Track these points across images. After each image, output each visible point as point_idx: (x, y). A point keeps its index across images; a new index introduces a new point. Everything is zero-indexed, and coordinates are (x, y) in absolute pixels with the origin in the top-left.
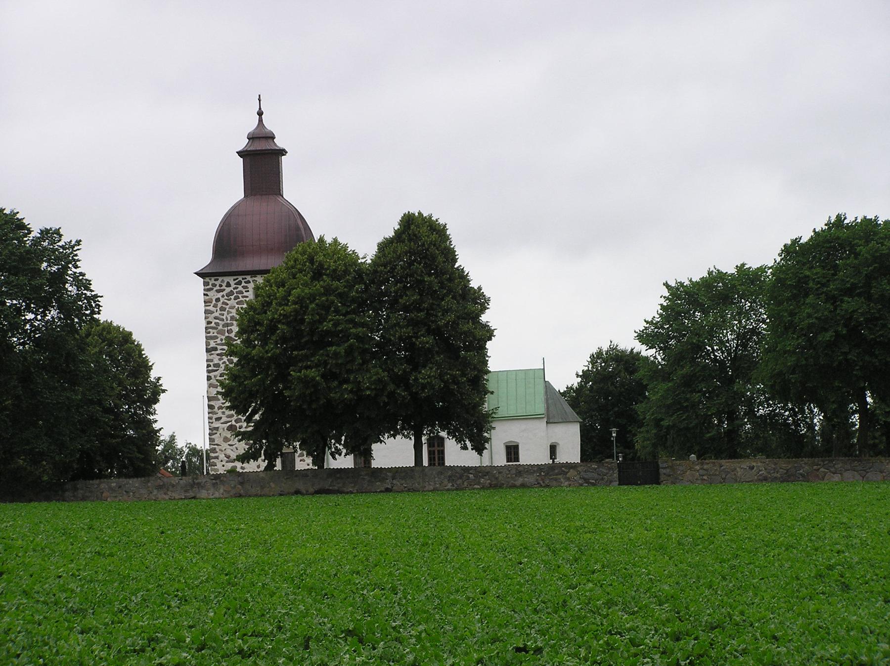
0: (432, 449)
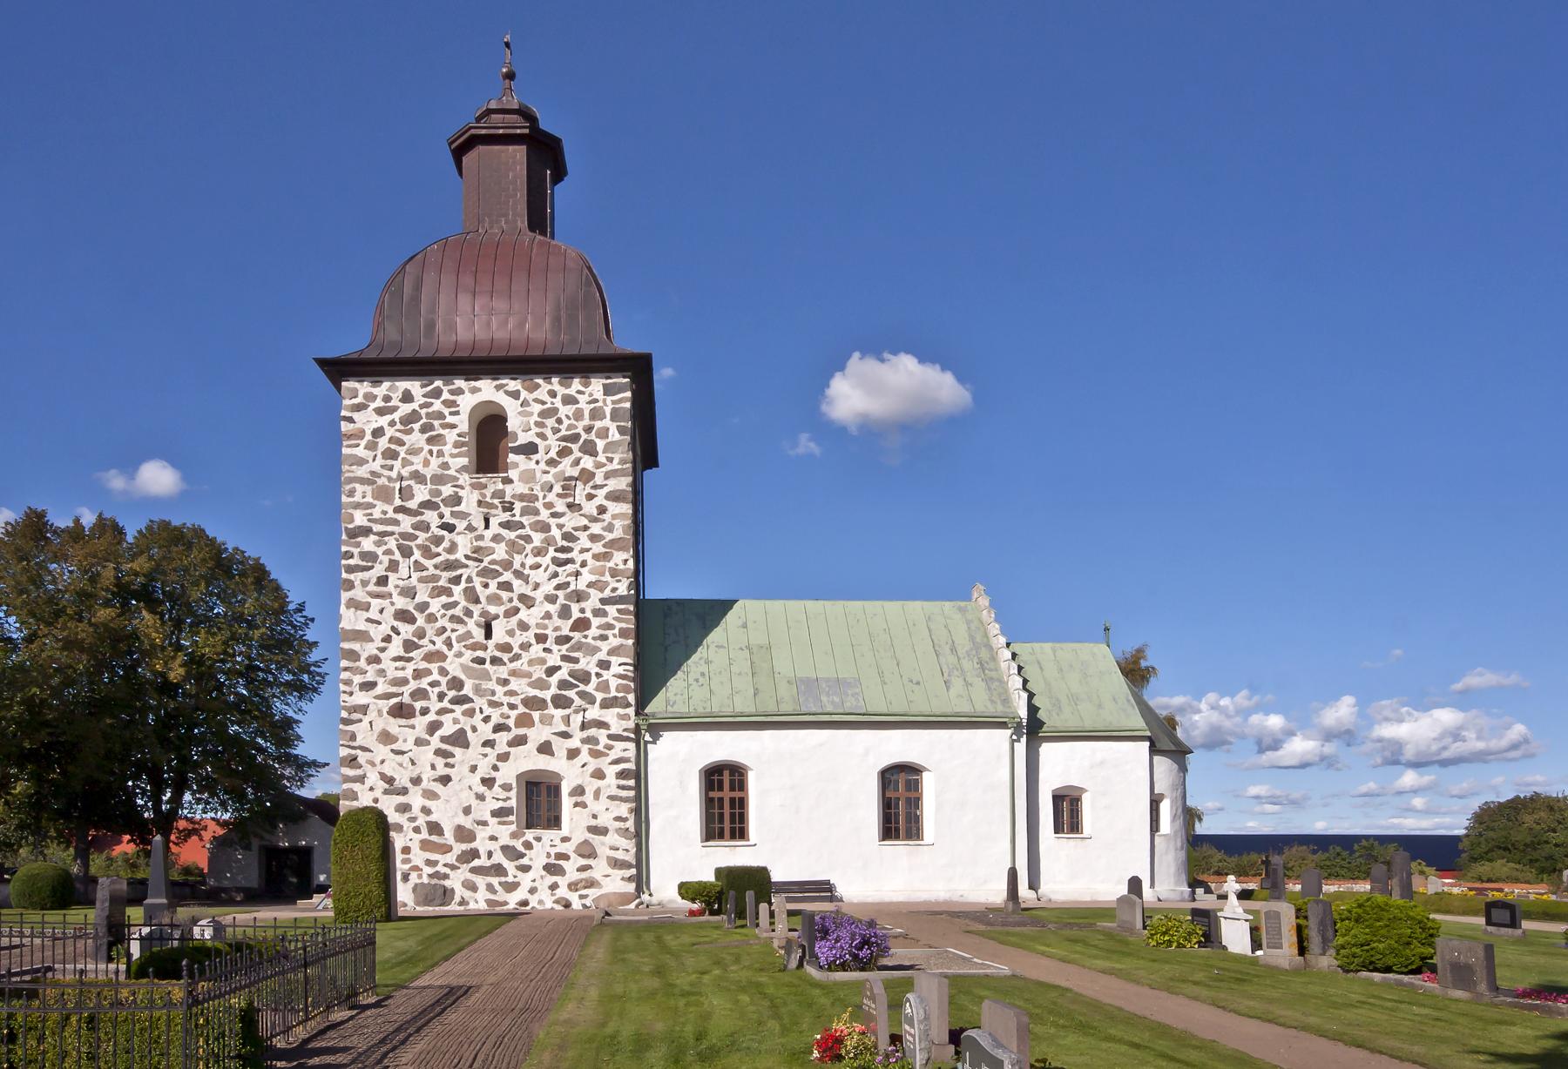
0: (737, 794)
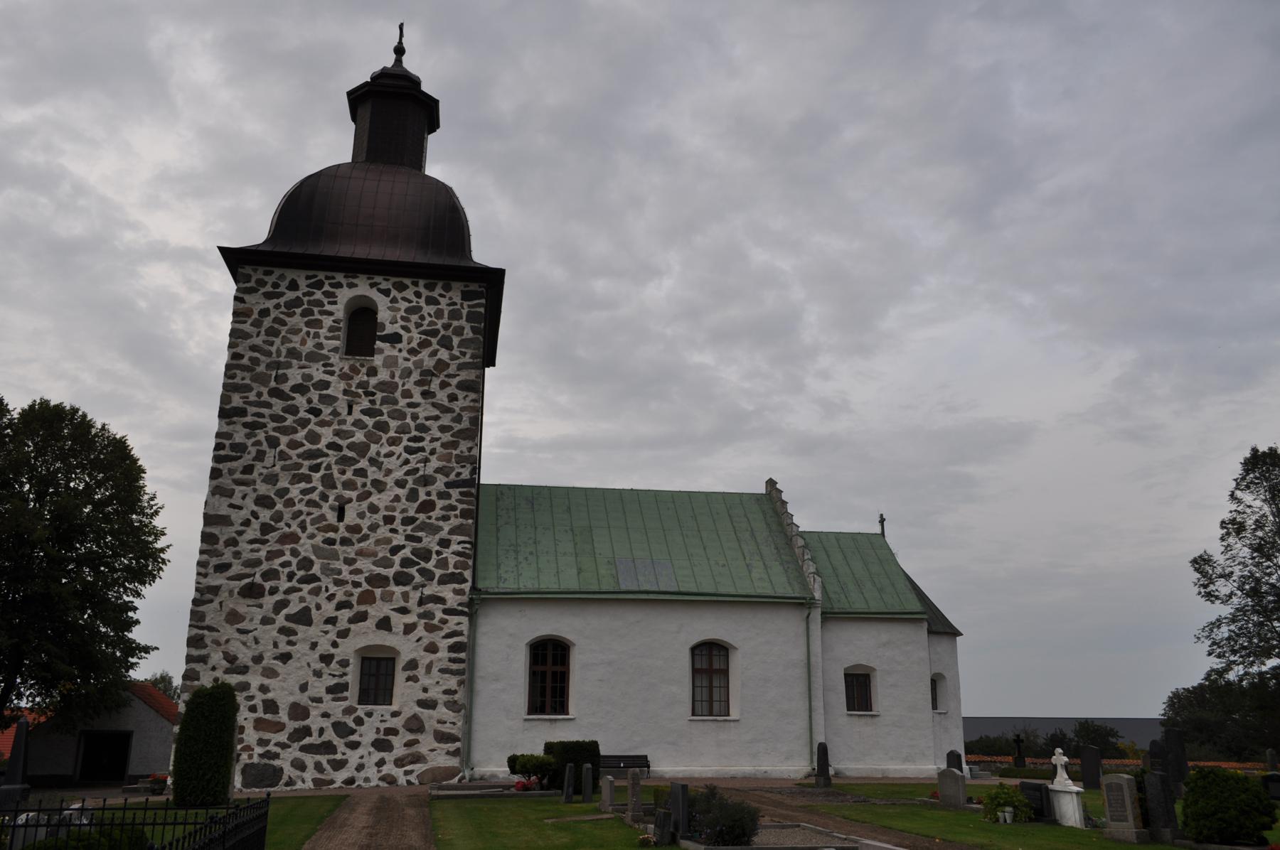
0: (559, 669)
